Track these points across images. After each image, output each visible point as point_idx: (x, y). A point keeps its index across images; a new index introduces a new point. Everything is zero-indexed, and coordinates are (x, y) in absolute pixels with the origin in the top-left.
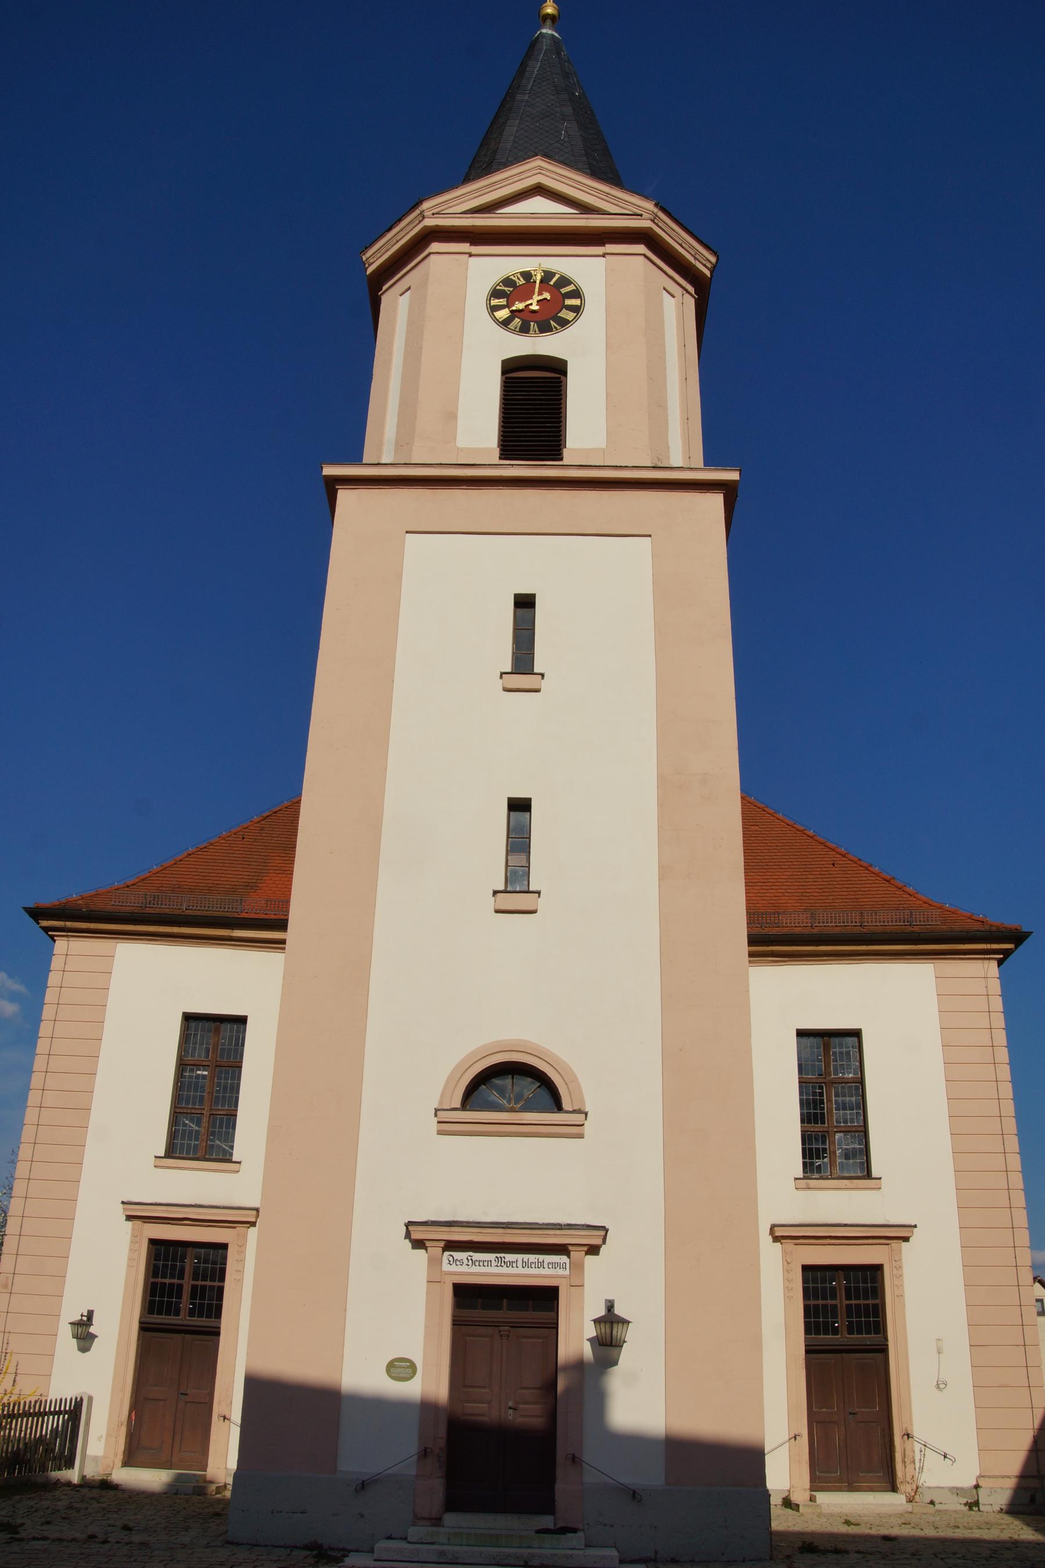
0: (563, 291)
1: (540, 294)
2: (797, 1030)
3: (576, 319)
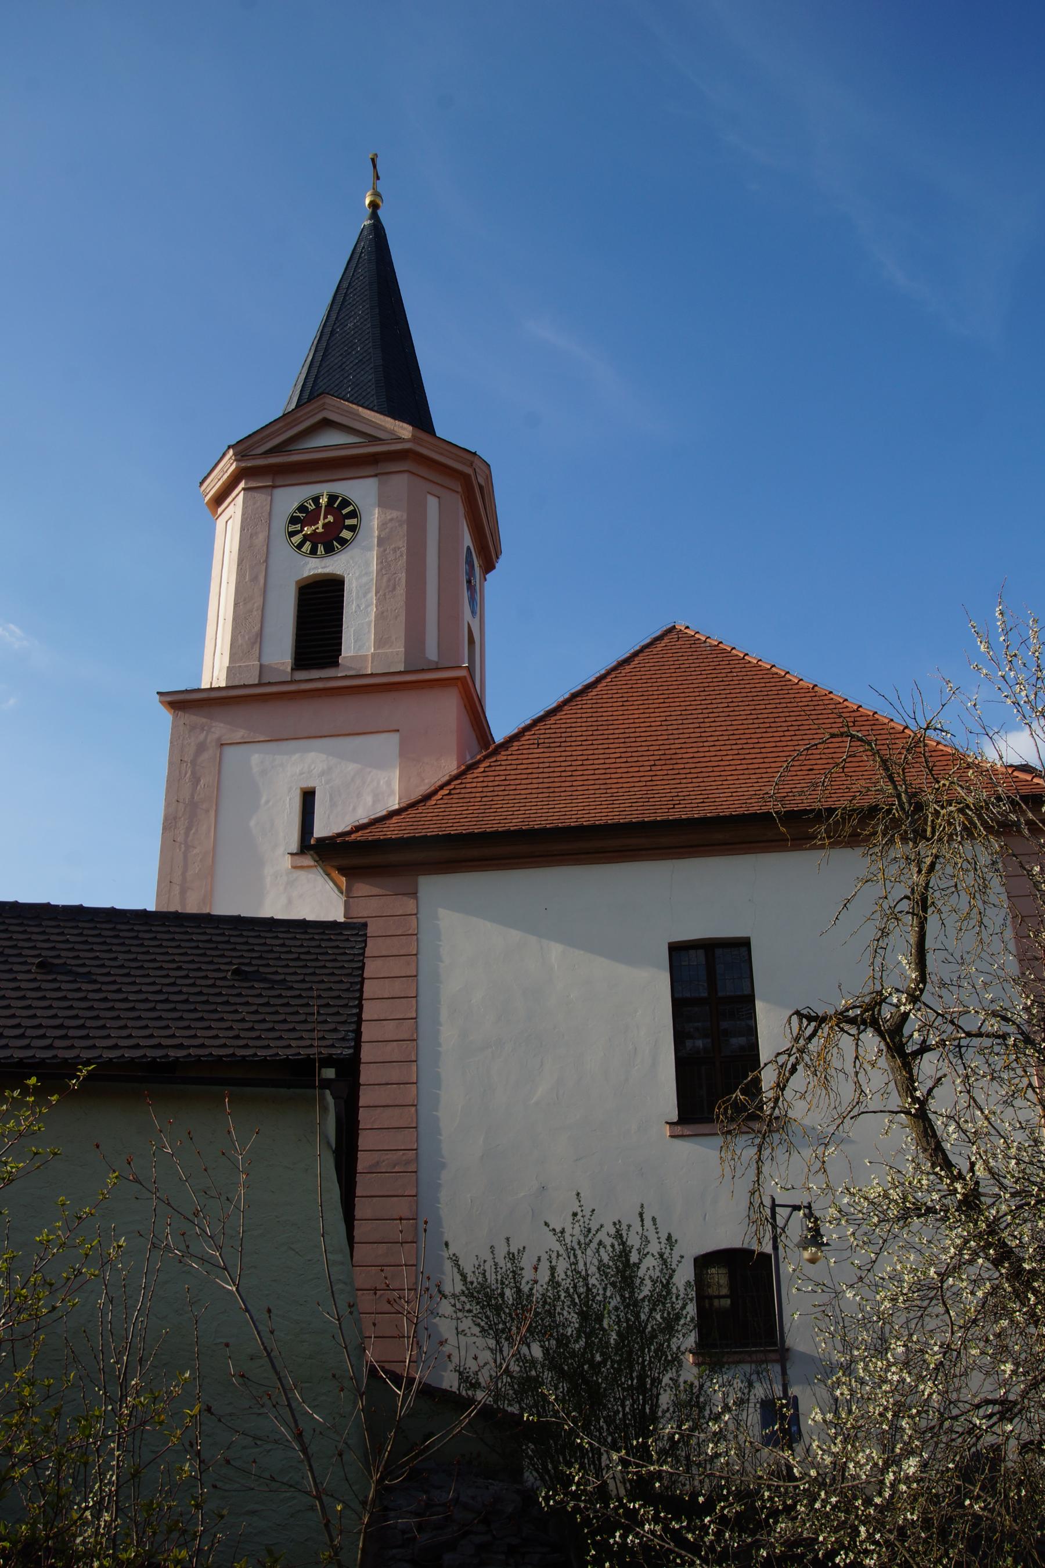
0: (344, 512)
1: (325, 517)
2: (739, 948)
3: (353, 538)
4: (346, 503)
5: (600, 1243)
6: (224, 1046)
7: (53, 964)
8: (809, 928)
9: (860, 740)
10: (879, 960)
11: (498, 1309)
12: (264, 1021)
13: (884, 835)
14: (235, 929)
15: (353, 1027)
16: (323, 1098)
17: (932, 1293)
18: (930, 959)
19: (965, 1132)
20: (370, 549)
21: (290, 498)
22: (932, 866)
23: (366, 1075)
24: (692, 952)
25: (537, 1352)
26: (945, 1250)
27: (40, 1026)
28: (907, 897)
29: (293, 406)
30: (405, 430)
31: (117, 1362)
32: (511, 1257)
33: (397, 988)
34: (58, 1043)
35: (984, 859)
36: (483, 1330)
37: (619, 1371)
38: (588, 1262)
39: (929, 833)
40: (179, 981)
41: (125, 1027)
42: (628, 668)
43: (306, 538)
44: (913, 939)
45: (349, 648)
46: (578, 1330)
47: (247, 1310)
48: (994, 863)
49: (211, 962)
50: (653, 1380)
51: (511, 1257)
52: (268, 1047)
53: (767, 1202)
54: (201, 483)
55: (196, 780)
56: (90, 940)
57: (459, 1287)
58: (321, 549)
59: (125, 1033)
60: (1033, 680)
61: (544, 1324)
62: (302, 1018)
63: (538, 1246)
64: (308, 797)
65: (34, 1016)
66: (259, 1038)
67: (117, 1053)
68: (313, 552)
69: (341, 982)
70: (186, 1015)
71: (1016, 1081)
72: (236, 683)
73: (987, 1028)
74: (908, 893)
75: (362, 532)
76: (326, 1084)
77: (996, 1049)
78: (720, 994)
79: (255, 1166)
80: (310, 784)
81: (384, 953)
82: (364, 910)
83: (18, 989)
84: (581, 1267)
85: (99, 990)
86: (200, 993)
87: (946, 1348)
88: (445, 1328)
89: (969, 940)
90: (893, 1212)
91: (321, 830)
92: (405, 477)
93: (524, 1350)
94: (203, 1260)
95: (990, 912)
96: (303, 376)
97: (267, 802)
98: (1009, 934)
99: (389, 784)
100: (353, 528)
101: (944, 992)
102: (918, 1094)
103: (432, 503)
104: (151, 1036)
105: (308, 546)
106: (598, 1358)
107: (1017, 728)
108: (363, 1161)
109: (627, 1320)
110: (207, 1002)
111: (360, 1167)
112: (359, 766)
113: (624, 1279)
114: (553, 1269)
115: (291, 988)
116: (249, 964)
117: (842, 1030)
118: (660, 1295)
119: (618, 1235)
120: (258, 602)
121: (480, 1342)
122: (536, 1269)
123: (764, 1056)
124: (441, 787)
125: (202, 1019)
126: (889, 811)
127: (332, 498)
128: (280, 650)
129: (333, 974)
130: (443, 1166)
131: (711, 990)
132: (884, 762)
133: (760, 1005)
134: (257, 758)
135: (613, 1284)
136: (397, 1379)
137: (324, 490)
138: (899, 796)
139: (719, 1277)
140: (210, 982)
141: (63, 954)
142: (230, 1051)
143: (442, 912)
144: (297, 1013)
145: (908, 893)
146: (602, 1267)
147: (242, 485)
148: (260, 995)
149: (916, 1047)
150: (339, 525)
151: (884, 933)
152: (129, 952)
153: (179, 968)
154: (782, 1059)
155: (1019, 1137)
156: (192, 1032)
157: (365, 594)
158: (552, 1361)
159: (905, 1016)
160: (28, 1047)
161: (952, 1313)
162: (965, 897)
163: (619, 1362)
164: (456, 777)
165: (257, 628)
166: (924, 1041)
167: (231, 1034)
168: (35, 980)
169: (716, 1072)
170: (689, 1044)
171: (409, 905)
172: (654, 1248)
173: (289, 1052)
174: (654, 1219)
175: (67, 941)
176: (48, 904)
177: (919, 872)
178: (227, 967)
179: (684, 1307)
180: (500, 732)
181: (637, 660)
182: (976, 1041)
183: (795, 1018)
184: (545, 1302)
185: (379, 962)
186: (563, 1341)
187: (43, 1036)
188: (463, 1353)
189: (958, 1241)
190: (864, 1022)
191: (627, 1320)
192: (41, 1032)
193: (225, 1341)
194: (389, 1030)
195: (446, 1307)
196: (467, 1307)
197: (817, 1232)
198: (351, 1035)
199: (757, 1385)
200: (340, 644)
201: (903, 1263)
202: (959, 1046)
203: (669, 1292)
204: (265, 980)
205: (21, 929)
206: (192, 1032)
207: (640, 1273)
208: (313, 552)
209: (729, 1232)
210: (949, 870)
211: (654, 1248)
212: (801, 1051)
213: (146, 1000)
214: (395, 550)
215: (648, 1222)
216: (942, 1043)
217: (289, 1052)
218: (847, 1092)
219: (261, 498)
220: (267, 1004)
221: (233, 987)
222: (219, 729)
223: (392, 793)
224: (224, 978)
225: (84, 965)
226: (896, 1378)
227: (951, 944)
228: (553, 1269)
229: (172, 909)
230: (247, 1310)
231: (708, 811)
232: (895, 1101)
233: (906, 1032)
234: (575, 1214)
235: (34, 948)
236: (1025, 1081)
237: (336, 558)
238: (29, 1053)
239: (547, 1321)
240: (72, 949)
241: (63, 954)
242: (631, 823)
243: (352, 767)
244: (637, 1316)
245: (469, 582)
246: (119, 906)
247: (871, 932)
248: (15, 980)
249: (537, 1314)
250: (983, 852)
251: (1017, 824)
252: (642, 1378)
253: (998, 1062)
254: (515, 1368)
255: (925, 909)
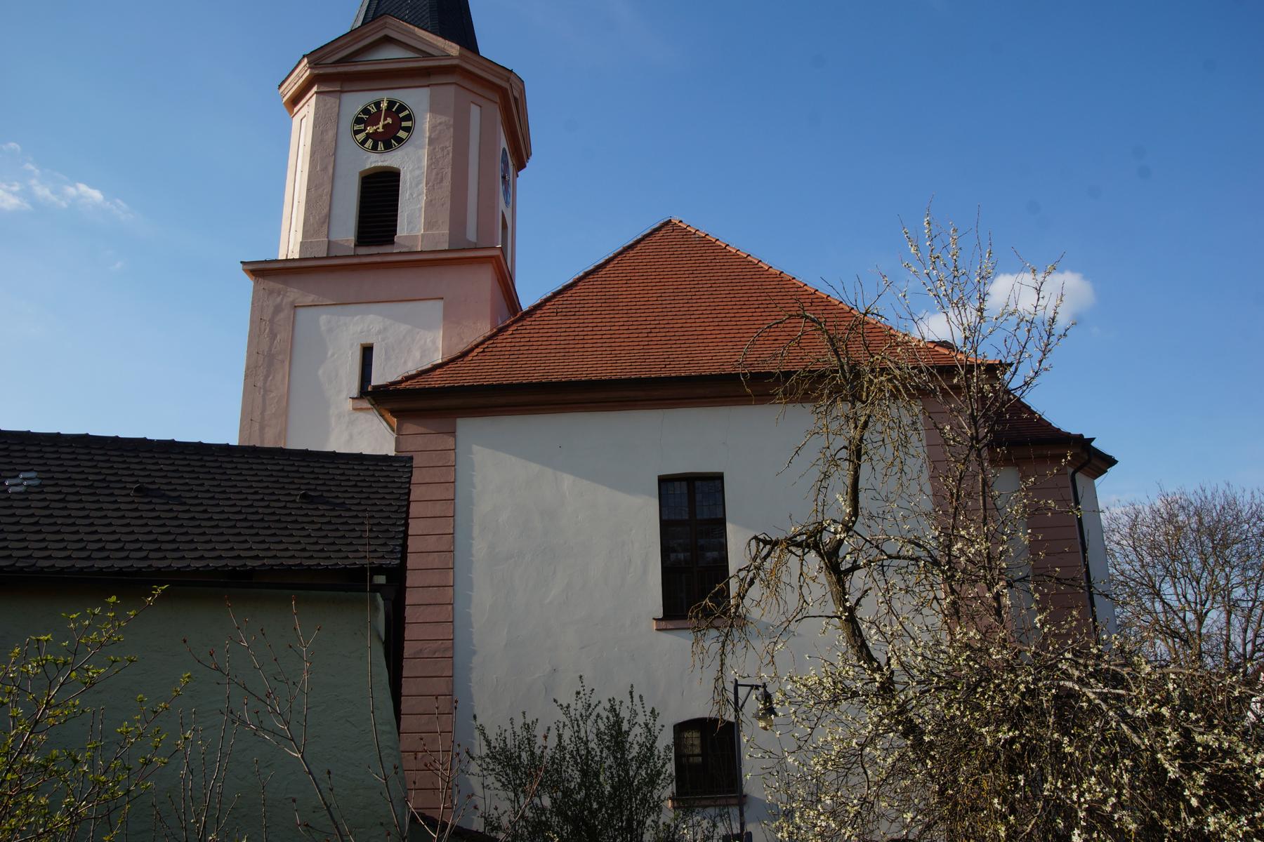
3: (409, 138)
4: (402, 108)
5: (598, 716)
6: (293, 557)
7: (148, 489)
8: (770, 466)
9: (813, 321)
10: (821, 497)
11: (515, 769)
12: (326, 536)
13: (829, 398)
14: (303, 460)
15: (400, 542)
16: (374, 600)
17: (853, 759)
18: (862, 496)
19: (883, 634)
20: (423, 148)
21: (356, 102)
22: (866, 423)
23: (411, 579)
24: (677, 484)
25: (547, 801)
26: (865, 726)
27: (137, 541)
28: (845, 447)
29: (359, 24)
30: (453, 49)
31: (196, 822)
32: (527, 727)
33: (437, 509)
34: (152, 555)
35: (906, 420)
36: (503, 785)
37: (611, 816)
38: (589, 730)
39: (864, 398)
40: (256, 504)
41: (210, 541)
42: (632, 253)
43: (368, 136)
44: (849, 481)
45: (403, 230)
46: (580, 785)
47: (310, 773)
48: (914, 423)
49: (283, 488)
50: (639, 823)
51: (527, 727)
52: (330, 558)
53: (730, 687)
54: (280, 86)
55: (273, 335)
56: (181, 469)
57: (485, 750)
58: (381, 146)
59: (209, 546)
60: (951, 278)
61: (553, 781)
62: (358, 534)
63: (547, 717)
64: (367, 351)
65: (132, 533)
66: (322, 550)
67: (203, 563)
68: (375, 148)
69: (391, 505)
70: (261, 532)
71: (924, 594)
72: (308, 256)
73: (904, 553)
74: (846, 443)
75: (415, 133)
76: (377, 588)
77: (911, 568)
78: (699, 517)
79: (322, 654)
80: (368, 341)
81: (427, 480)
82: (411, 445)
83: (118, 509)
84: (582, 734)
85: (188, 511)
86: (273, 514)
87: (864, 801)
88: (475, 783)
89: (893, 484)
90: (826, 696)
91: (377, 379)
92: (452, 89)
93: (536, 800)
94: (273, 733)
95: (910, 461)
96: (365, 8)
97: (333, 355)
98: (925, 477)
99: (434, 342)
100: (408, 129)
101: (872, 523)
102: (848, 604)
103: (475, 111)
104: (232, 549)
105: (370, 143)
106: (595, 806)
107: (934, 312)
108: (409, 649)
109: (619, 776)
110: (279, 521)
111: (406, 654)
112: (409, 327)
113: (617, 743)
114: (560, 736)
115: (350, 510)
116: (315, 490)
117: (791, 552)
118: (645, 756)
119: (613, 709)
120: (327, 188)
121: (502, 794)
122: (546, 737)
123: (732, 570)
124: (477, 346)
125: (275, 535)
126: (834, 378)
127: (391, 103)
128: (345, 230)
129: (384, 498)
130: (474, 653)
131: (691, 517)
132: (831, 340)
133: (730, 527)
134: (324, 318)
135: (608, 748)
136: (432, 823)
137: (384, 96)
138: (842, 367)
139: (693, 737)
140: (282, 504)
141: (157, 480)
142: (298, 561)
143: (475, 448)
144: (354, 530)
145: (846, 443)
146: (599, 734)
147: (315, 89)
148: (323, 516)
149: (849, 566)
150: (396, 126)
151: (826, 476)
152: (214, 479)
153: (256, 493)
154: (742, 574)
155: (926, 637)
156: (266, 546)
157: (417, 185)
158: (558, 809)
159: (841, 542)
160: (127, 558)
161: (869, 772)
162: (890, 448)
163: (612, 809)
164: (490, 338)
165: (326, 210)
166: (855, 561)
167: (299, 547)
168: (133, 502)
169: (695, 581)
170: (673, 556)
171: (449, 442)
172: (641, 719)
173: (347, 562)
174: (641, 697)
175: (161, 470)
176: (145, 439)
177: (856, 427)
178: (295, 492)
179: (664, 765)
180: (526, 303)
181: (639, 246)
182: (896, 562)
183: (753, 543)
184: (553, 763)
185: (423, 488)
186: (567, 793)
187: (140, 549)
188: (488, 802)
189: (875, 719)
190: (808, 546)
191: (619, 776)
192: (138, 546)
193: (294, 796)
194: (431, 543)
195: (474, 767)
196: (491, 767)
197: (770, 711)
198: (398, 549)
199: (720, 824)
200: (396, 226)
201: (832, 736)
202: (882, 566)
203: (652, 754)
204: (327, 503)
205: (120, 459)
206: (266, 546)
207: (630, 739)
208: (375, 148)
209: (701, 707)
210: (879, 427)
211: (641, 719)
212: (758, 568)
213: (228, 519)
214: (443, 149)
215: (636, 698)
216: (868, 564)
217: (347, 562)
218: (792, 600)
219: (331, 100)
220: (329, 523)
221: (301, 508)
222: (294, 293)
223: (437, 349)
224: (294, 501)
225: (175, 490)
226: (824, 824)
227: (878, 485)
228: (560, 736)
229: (252, 444)
230: (310, 773)
231: (693, 371)
232: (831, 608)
233: (841, 554)
234: (578, 693)
235: (132, 475)
236: (931, 595)
237: (393, 153)
238: (128, 563)
239: (555, 777)
240: (165, 477)
241: (157, 480)
242: (630, 379)
243: (404, 328)
244: (627, 774)
245: (504, 177)
246: (205, 441)
247: (816, 474)
248: (115, 502)
249: (547, 772)
250: (907, 413)
251: (933, 391)
252: (630, 821)
253: (912, 580)
254: (529, 814)
255: (859, 458)
